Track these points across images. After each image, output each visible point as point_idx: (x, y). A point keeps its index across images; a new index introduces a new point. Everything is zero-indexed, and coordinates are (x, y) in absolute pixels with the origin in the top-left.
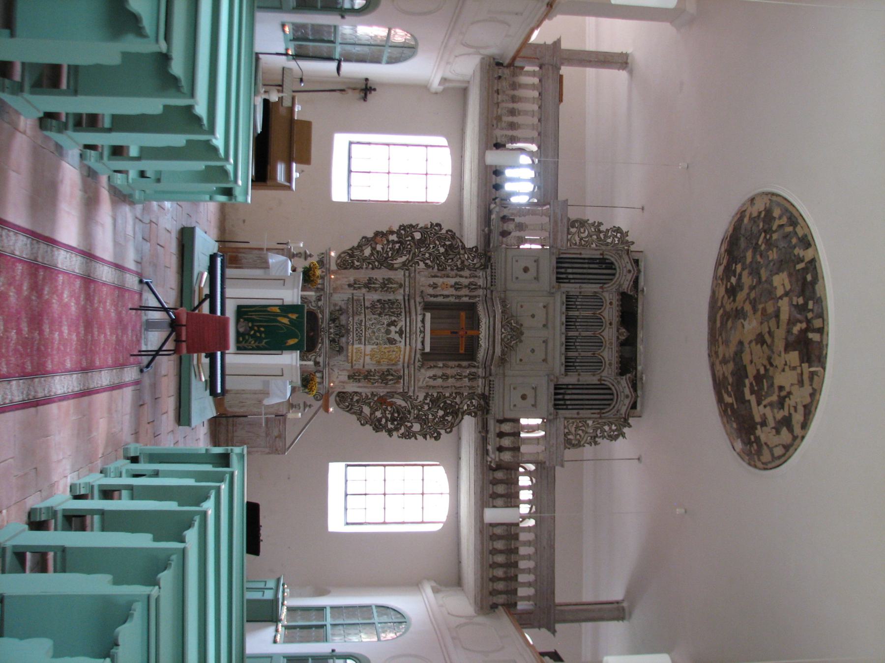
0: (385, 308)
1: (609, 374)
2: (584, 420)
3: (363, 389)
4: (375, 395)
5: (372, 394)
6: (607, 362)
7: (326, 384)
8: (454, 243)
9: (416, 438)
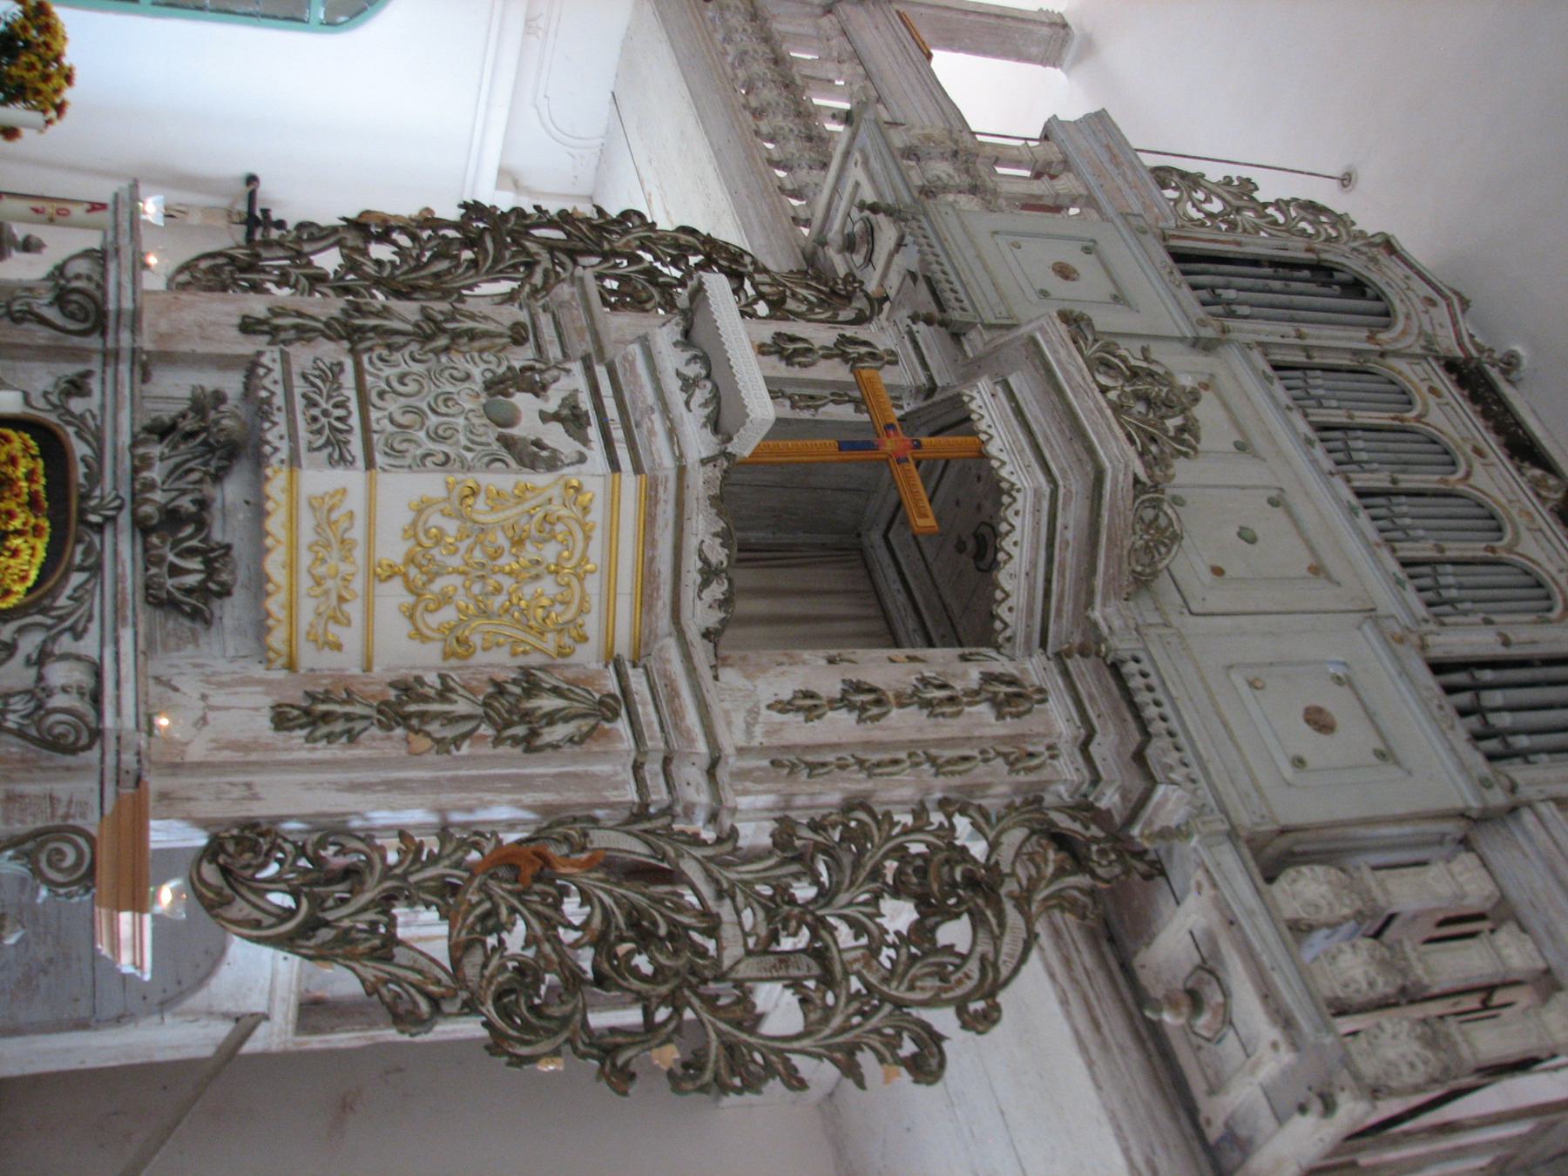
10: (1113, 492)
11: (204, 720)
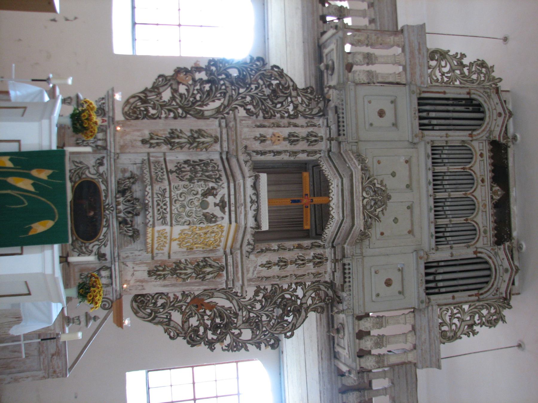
0: (194, 170)
1: (484, 243)
2: (458, 305)
3: (172, 288)
4: (187, 296)
5: (183, 294)
6: (482, 230)
7: (116, 285)
8: (283, 82)
9: (247, 350)
10: (355, 229)
11: (133, 274)
